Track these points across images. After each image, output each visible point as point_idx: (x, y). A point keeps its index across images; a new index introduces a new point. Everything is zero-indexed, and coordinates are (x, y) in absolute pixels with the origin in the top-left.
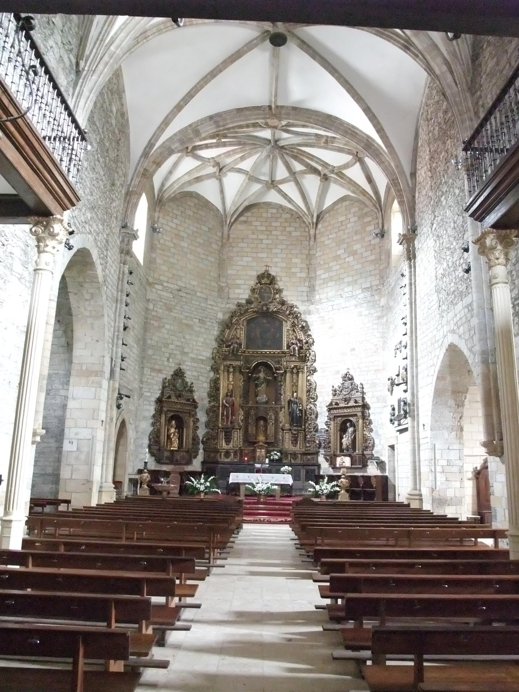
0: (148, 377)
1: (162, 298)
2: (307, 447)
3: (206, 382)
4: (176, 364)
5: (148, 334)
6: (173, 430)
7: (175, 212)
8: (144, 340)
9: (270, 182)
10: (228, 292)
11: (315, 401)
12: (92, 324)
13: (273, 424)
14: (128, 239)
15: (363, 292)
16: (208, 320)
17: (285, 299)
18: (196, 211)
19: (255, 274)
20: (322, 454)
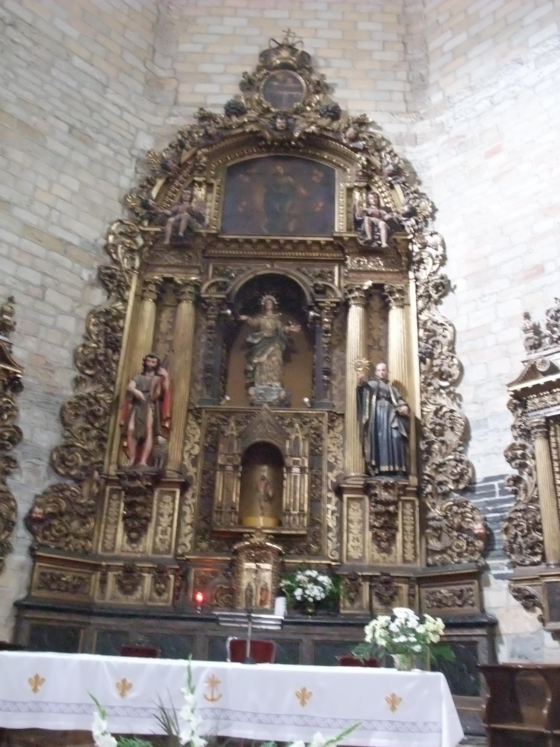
2: (430, 552)
3: (72, 313)
10: (176, 90)
11: (455, 383)
16: (102, 139)
19: (255, 51)
20: (498, 577)
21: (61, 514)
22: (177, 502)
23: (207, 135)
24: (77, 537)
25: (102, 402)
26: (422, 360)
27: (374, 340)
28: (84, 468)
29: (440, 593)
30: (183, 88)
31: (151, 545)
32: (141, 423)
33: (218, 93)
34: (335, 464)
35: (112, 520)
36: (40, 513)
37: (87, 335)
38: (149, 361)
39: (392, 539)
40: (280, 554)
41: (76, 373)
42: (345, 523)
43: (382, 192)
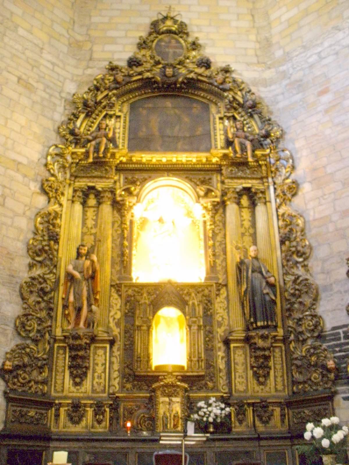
10: (91, 50)
11: (305, 259)
13: (199, 327)
19: (147, 21)
21: (25, 366)
22: (108, 354)
23: (116, 81)
24: (37, 383)
25: (48, 282)
26: (282, 243)
27: (245, 228)
28: (38, 331)
29: (304, 413)
31: (91, 387)
32: (78, 296)
33: (122, 53)
34: (222, 322)
35: (60, 370)
36: (10, 366)
37: (35, 231)
38: (81, 249)
39: (267, 376)
40: (186, 390)
41: (29, 260)
42: (233, 365)
43: (245, 120)
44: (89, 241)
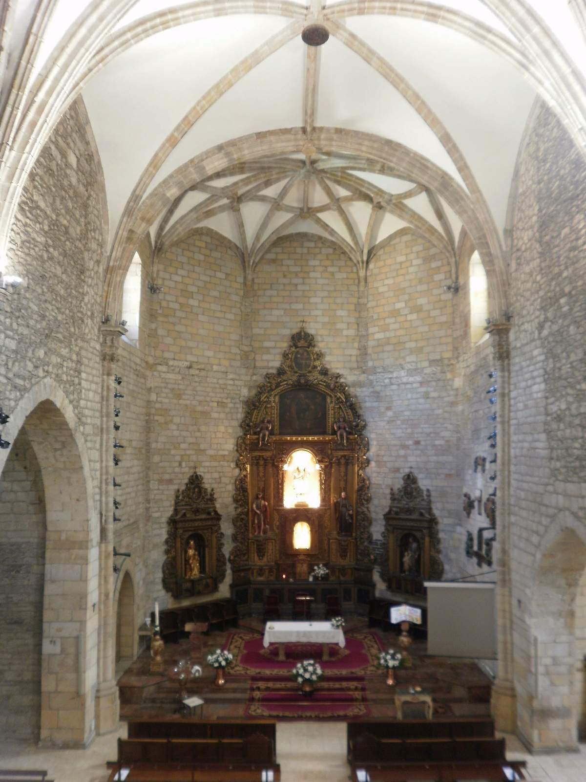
0: (155, 492)
1: (167, 383)
4: (190, 468)
5: (153, 436)
6: (191, 552)
7: (179, 259)
8: (148, 444)
9: (305, 210)
12: (68, 478)
14: (111, 337)
15: (430, 366)
17: (328, 366)
18: (208, 253)
19: (287, 332)
30: (258, 357)
39: (346, 556)
44: (262, 484)
